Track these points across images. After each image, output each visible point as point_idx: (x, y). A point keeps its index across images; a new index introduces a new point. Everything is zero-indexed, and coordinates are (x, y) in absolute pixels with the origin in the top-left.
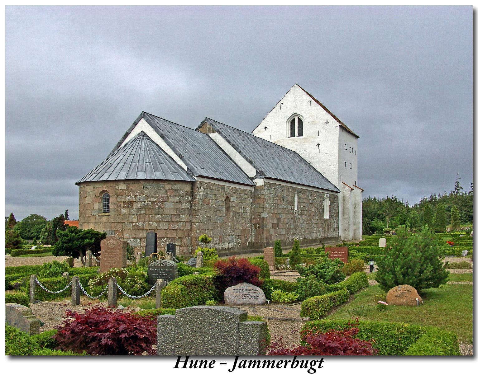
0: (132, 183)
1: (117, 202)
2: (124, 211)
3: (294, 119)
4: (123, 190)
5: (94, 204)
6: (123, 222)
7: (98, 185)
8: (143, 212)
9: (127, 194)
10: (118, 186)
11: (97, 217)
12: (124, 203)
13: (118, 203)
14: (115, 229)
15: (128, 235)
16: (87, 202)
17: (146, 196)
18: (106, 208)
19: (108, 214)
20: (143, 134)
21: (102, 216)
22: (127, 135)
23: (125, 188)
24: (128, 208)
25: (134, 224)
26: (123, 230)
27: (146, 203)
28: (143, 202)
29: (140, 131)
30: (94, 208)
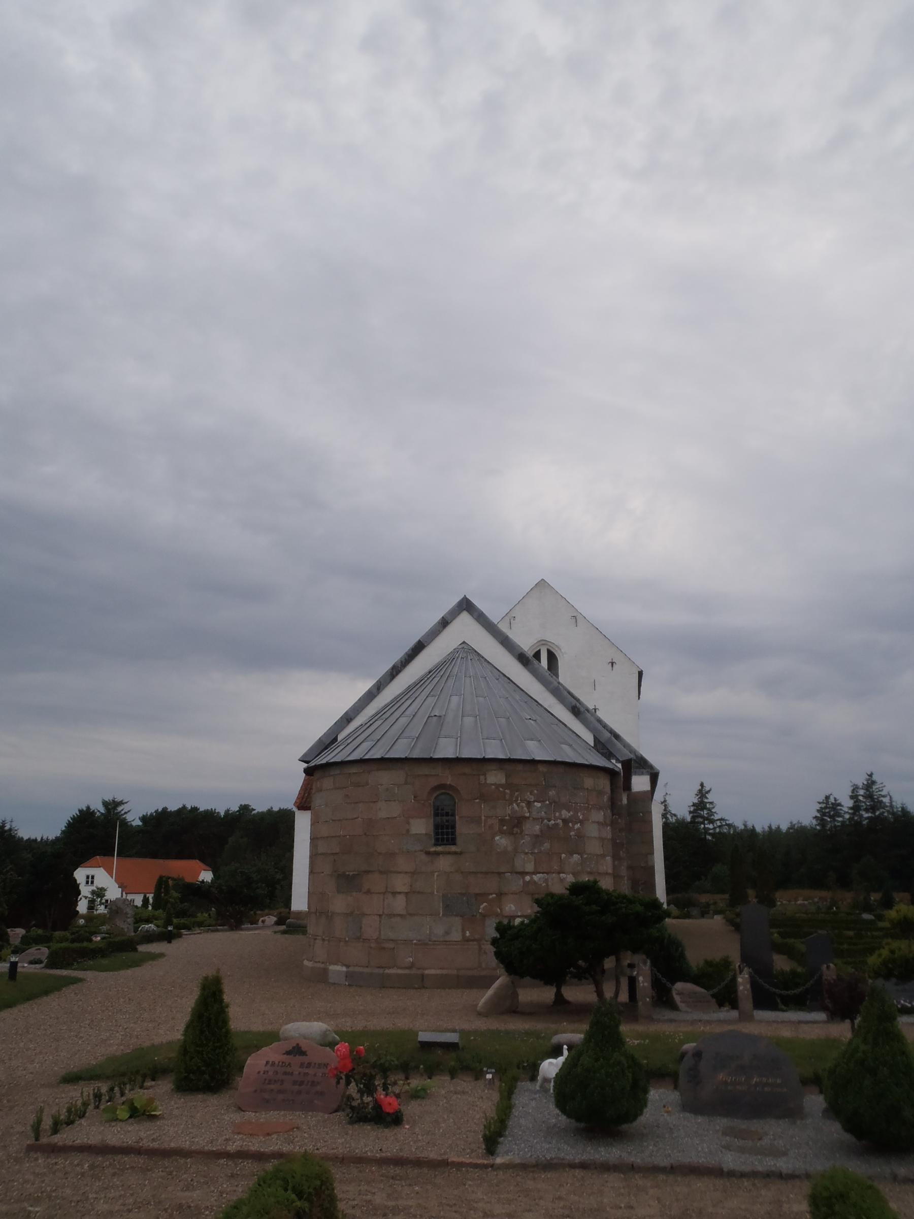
0: (520, 767)
1: (483, 818)
2: (502, 841)
3: (539, 651)
4: (498, 786)
5: (411, 821)
6: (499, 874)
7: (425, 770)
8: (547, 845)
9: (507, 797)
10: (485, 775)
11: (423, 857)
12: (502, 822)
13: (485, 821)
14: (477, 891)
15: (513, 908)
16: (383, 814)
17: (551, 804)
18: (445, 833)
19: (453, 848)
20: (466, 651)
21: (437, 854)
22: (418, 648)
23: (503, 781)
24: (513, 834)
25: (528, 878)
26: (500, 895)
27: (553, 822)
28: (546, 821)
29: (455, 644)
30: (408, 831)
